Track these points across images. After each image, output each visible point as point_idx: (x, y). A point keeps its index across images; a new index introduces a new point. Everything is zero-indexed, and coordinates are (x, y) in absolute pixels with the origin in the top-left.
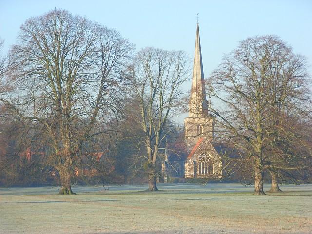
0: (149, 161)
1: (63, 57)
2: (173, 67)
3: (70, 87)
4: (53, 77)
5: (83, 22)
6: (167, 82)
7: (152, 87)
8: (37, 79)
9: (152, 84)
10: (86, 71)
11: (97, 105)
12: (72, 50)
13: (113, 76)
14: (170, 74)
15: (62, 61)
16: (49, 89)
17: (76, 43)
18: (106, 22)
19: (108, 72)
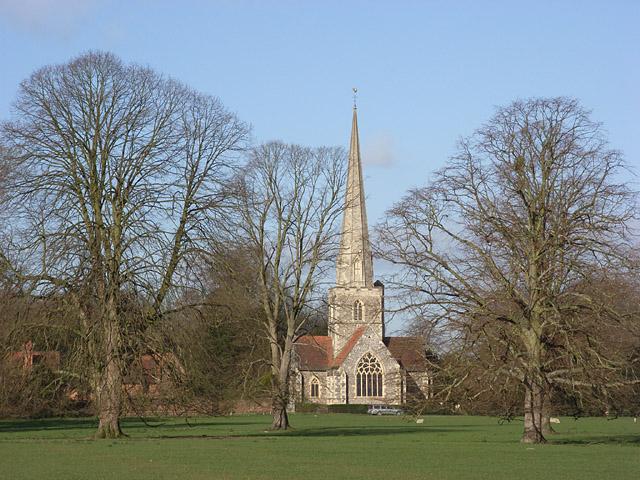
0: (274, 371)
1: (107, 151)
2: (321, 181)
3: (119, 214)
4: (83, 191)
5: (146, 77)
6: (312, 210)
7: (280, 219)
8: (50, 196)
9: (280, 214)
10: (151, 180)
11: (176, 250)
12: (124, 137)
13: (209, 188)
14: (317, 195)
15: (105, 159)
16: (76, 218)
17: (132, 122)
18: (200, 86)
19: (199, 182)
